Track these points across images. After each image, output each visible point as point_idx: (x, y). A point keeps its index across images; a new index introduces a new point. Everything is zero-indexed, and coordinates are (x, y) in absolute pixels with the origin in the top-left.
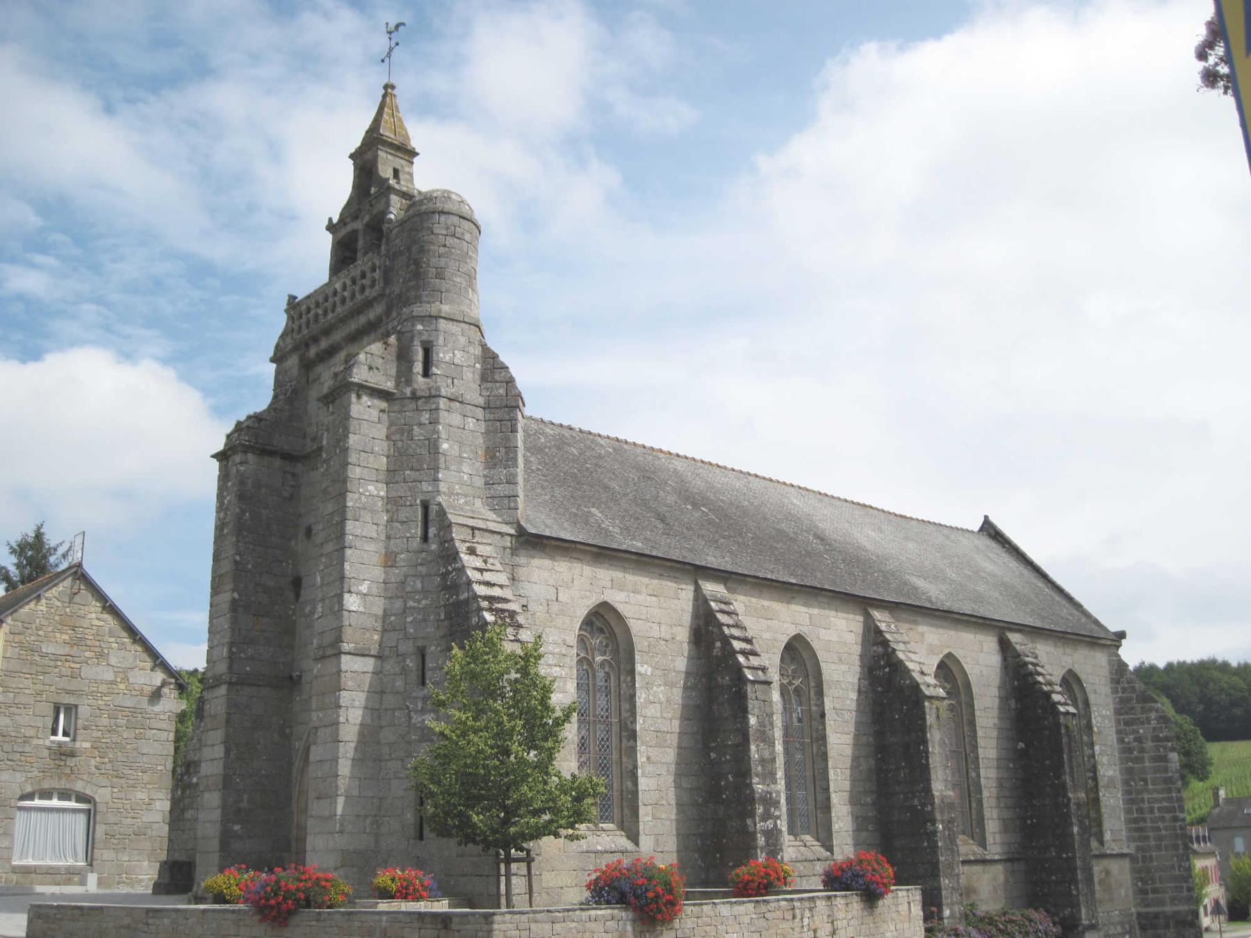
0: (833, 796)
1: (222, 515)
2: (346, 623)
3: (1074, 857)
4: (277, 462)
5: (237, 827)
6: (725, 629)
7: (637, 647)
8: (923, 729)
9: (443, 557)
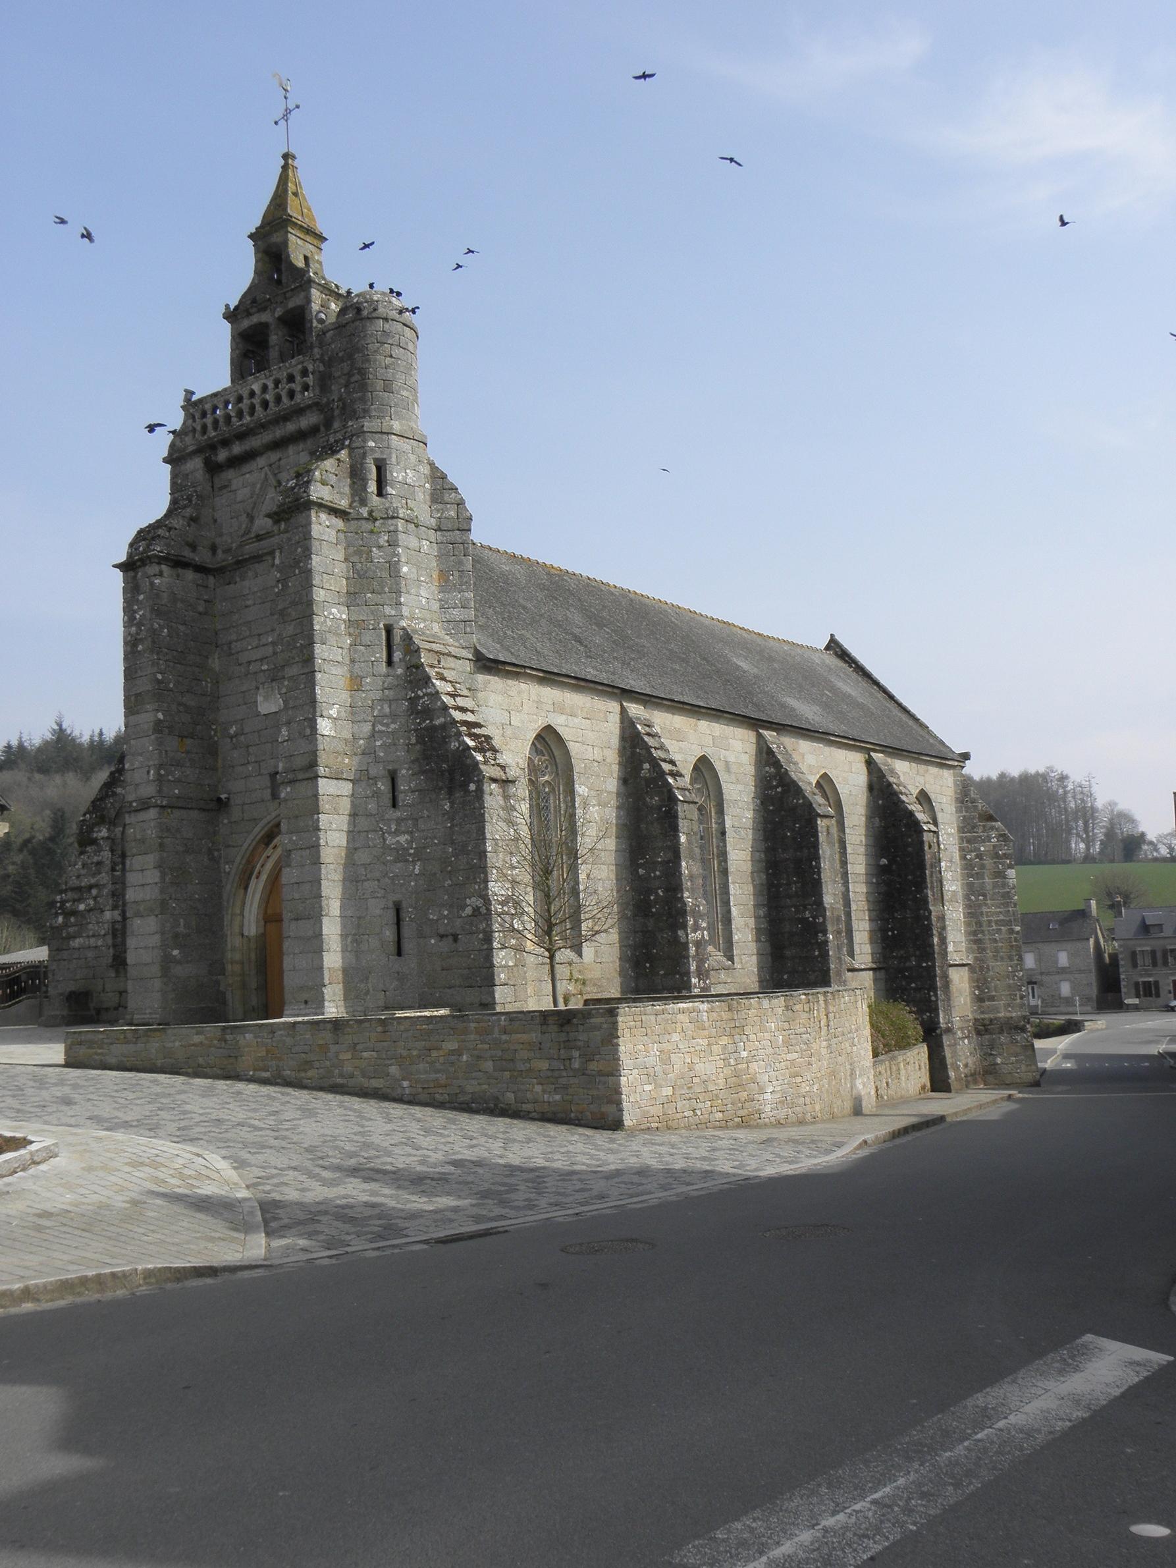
0: (733, 909)
1: (133, 629)
2: (320, 747)
3: (934, 966)
4: (190, 575)
5: (175, 952)
6: (653, 750)
7: (576, 769)
8: (815, 846)
9: (410, 682)
